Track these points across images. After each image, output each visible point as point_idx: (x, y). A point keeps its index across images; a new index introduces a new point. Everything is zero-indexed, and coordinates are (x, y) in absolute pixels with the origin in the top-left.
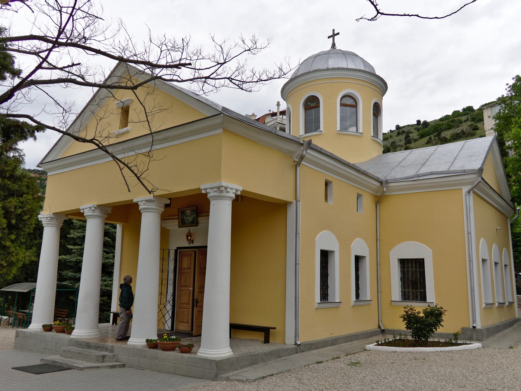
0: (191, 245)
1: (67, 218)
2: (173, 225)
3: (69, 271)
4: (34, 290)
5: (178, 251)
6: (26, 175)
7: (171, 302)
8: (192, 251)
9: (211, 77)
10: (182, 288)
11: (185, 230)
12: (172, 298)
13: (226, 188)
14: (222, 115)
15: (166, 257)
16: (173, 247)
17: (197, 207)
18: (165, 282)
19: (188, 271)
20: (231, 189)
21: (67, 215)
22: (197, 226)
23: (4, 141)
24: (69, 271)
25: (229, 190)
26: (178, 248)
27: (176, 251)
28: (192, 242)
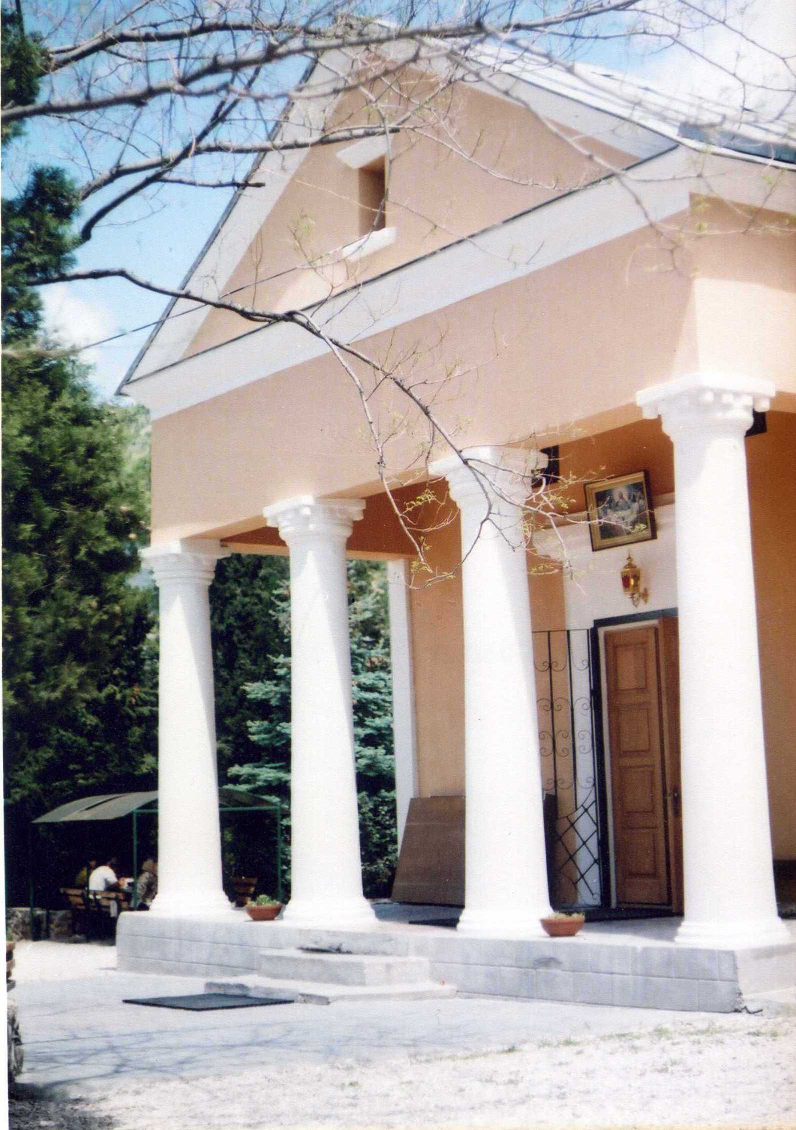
0: (643, 608)
1: (226, 553)
2: (570, 545)
3: (252, 734)
4: (154, 804)
5: (601, 631)
6: (145, 637)
7: (592, 811)
8: (647, 629)
9: (133, 378)
10: (627, 761)
11: (614, 560)
12: (592, 798)
13: (718, 394)
14: (681, 150)
15: (559, 656)
16: (579, 618)
17: (647, 475)
18: (563, 744)
19: (641, 698)
20: (737, 395)
21: (225, 541)
22: (654, 536)
23: (553, 929)
24: (252, 734)
25: (727, 399)
26: (599, 623)
27: (593, 635)
28: (645, 595)
